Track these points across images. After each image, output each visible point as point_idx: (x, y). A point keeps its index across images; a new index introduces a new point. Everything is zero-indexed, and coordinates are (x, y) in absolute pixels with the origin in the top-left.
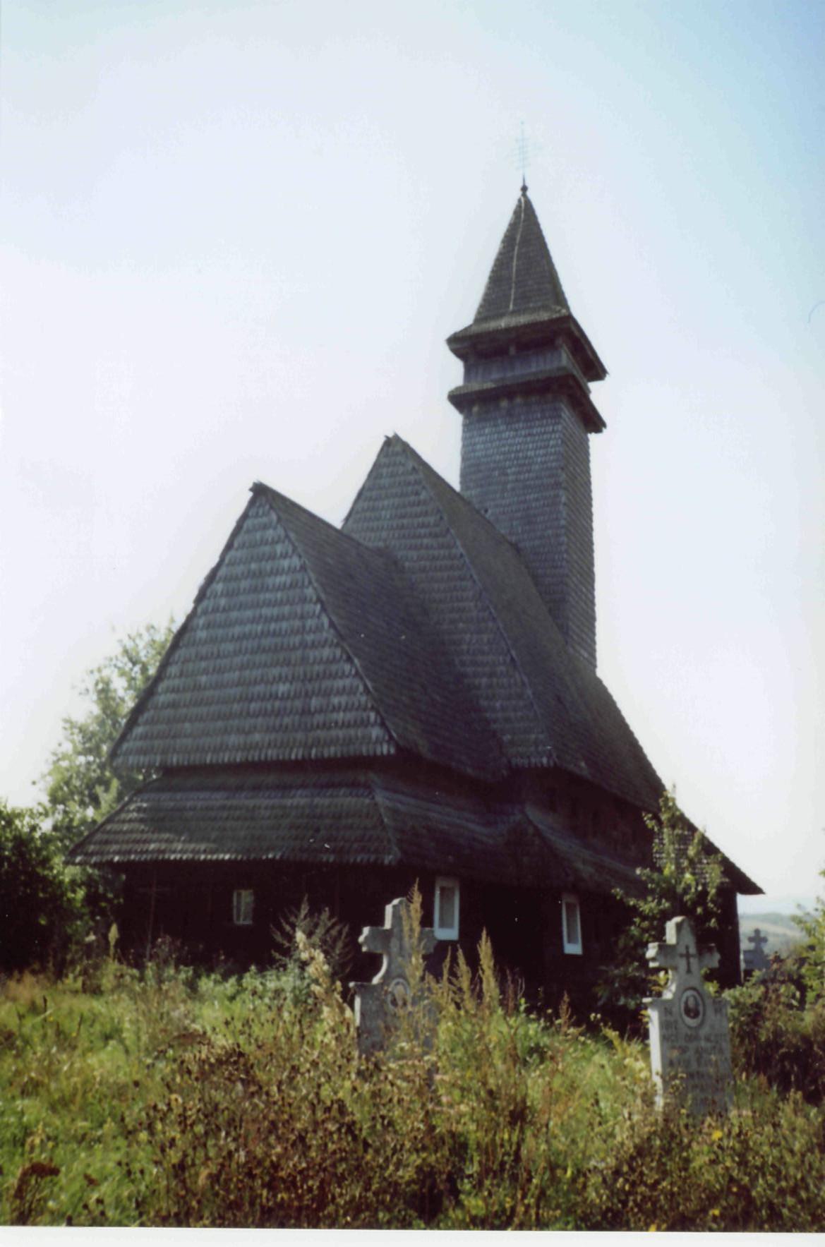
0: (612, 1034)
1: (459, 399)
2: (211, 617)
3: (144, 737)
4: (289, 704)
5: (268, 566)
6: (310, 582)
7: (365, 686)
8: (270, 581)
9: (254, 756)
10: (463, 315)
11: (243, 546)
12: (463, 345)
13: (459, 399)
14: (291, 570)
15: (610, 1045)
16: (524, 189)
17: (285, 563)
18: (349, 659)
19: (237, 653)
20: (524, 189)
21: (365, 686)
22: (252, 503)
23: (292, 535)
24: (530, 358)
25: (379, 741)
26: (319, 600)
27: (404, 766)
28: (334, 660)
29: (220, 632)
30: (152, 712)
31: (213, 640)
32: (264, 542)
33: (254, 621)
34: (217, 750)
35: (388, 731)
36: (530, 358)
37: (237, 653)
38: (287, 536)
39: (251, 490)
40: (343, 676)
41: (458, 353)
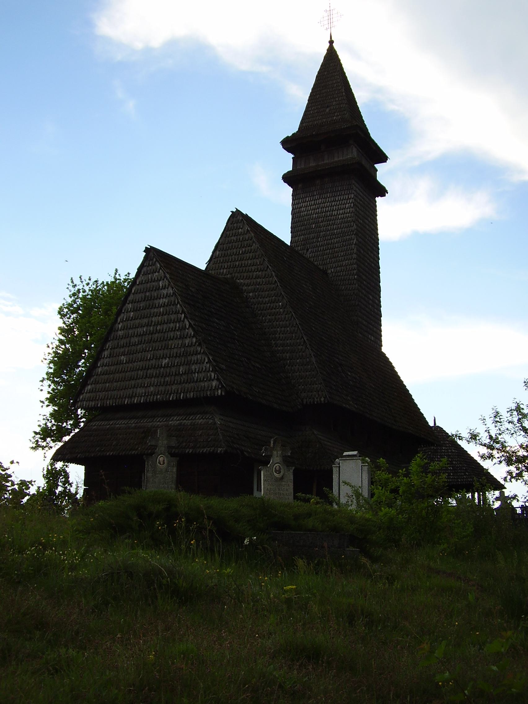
0: (127, 488)
1: (288, 178)
2: (125, 323)
3: (91, 391)
4: (168, 370)
5: (155, 294)
6: (178, 302)
7: (209, 358)
8: (156, 302)
9: (151, 399)
10: (292, 127)
11: (141, 283)
12: (288, 144)
13: (288, 178)
14: (168, 296)
15: (130, 493)
16: (331, 42)
17: (165, 292)
18: (200, 345)
19: (140, 343)
20: (331, 42)
21: (209, 358)
22: (146, 258)
23: (168, 276)
24: (335, 147)
25: (217, 388)
26: (183, 312)
27: (229, 403)
28: (191, 345)
29: (372, 288)
30: (95, 377)
31: (126, 336)
32: (153, 281)
33: (148, 325)
34: (131, 397)
35: (220, 383)
36: (335, 147)
37: (140, 343)
38: (165, 277)
39: (145, 251)
40: (197, 353)
41: (288, 150)
